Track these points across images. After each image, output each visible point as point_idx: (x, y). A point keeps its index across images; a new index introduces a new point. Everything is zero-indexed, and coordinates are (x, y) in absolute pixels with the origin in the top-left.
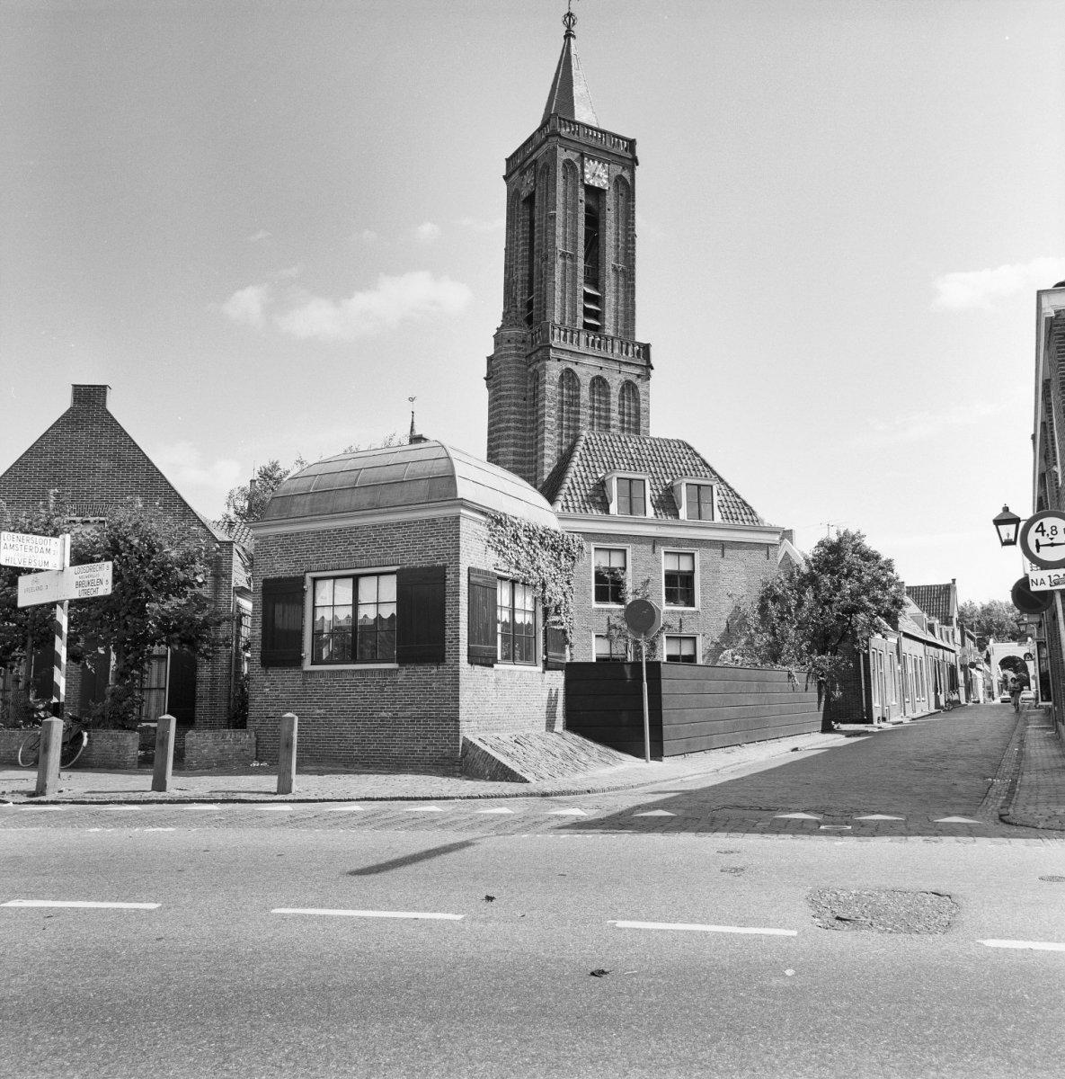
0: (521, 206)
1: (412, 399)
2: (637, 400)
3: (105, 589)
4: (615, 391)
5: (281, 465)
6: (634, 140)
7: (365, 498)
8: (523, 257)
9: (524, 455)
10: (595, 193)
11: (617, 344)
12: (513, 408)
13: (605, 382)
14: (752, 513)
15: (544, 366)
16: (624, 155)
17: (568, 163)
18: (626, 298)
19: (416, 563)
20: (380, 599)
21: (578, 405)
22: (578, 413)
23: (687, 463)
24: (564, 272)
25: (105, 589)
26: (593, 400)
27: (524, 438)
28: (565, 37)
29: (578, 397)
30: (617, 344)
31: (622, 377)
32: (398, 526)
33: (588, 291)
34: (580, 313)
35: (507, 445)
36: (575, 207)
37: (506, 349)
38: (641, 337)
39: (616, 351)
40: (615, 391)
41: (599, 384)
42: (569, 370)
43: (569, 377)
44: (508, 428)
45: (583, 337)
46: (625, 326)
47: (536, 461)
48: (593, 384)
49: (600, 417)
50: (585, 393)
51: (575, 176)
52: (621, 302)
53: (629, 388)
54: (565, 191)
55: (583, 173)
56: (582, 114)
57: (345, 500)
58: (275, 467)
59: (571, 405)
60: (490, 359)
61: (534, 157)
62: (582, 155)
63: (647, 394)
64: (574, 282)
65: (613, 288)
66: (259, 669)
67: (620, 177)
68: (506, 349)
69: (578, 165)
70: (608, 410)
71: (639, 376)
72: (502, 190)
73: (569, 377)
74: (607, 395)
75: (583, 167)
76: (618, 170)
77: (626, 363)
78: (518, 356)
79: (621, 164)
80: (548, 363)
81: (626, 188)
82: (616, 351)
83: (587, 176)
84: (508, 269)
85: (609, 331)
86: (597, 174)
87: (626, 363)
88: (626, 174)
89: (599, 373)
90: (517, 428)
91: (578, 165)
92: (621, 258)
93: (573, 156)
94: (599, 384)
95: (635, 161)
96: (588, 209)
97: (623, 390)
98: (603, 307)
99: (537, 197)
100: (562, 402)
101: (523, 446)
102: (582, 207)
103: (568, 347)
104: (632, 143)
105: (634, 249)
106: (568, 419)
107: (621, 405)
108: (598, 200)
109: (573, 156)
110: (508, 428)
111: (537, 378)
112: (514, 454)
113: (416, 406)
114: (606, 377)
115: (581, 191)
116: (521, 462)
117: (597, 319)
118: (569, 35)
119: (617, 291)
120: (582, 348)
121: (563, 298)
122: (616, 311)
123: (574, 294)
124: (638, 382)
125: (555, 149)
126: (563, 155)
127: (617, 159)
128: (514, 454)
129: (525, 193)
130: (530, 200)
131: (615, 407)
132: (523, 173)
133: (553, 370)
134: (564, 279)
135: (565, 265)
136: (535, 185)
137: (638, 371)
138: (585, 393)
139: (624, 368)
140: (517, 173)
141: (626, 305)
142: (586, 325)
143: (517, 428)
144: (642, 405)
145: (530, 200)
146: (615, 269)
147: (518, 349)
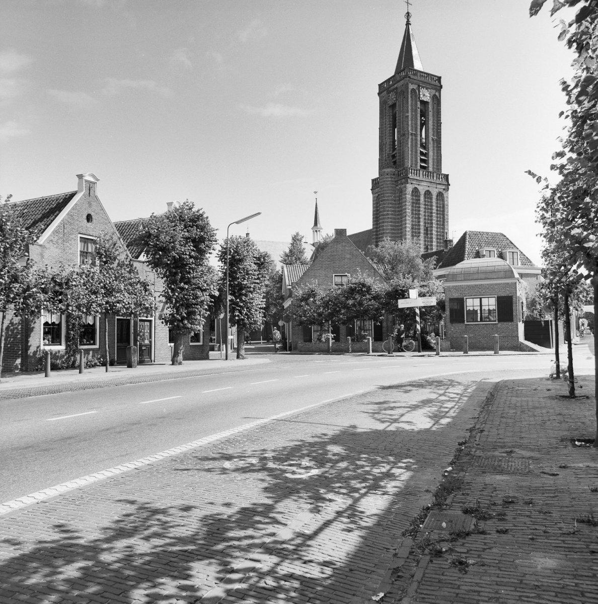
0: (387, 108)
1: (316, 192)
2: (443, 200)
3: (400, 301)
4: (434, 197)
5: (300, 234)
6: (440, 77)
7: (483, 276)
8: (389, 133)
9: (395, 226)
10: (424, 103)
11: (435, 175)
12: (390, 205)
13: (430, 193)
14: (531, 262)
15: (405, 187)
16: (435, 83)
17: (413, 89)
18: (437, 153)
19: (503, 295)
20: (490, 303)
21: (419, 204)
22: (420, 207)
23: (505, 243)
24: (412, 142)
25: (400, 301)
26: (425, 201)
27: (395, 219)
28: (406, 25)
29: (419, 200)
30: (435, 175)
31: (437, 190)
32: (496, 284)
33: (422, 150)
34: (419, 161)
35: (388, 222)
36: (416, 110)
37: (386, 178)
38: (444, 171)
39: (435, 178)
40: (434, 197)
41: (428, 194)
42: (416, 188)
43: (416, 191)
44: (388, 214)
45: (421, 172)
46: (437, 166)
47: (401, 229)
48: (425, 194)
49: (428, 209)
50: (422, 198)
51: (416, 96)
52: (435, 155)
53: (440, 196)
54: (412, 103)
55: (419, 94)
56: (418, 65)
57: (476, 277)
58: (298, 234)
59: (416, 204)
60: (375, 183)
61: (395, 86)
62: (419, 86)
63: (447, 197)
64: (416, 146)
65: (432, 148)
66: (449, 324)
67: (435, 95)
68: (386, 178)
69: (417, 91)
70: (432, 206)
71: (444, 189)
72: (377, 100)
73: (416, 191)
74: (431, 199)
75: (419, 91)
76: (433, 92)
77: (439, 184)
78: (391, 181)
79: (435, 89)
80: (407, 185)
81: (437, 100)
82: (435, 178)
83: (421, 96)
84: (381, 138)
85: (431, 169)
86: (426, 95)
87: (439, 184)
88: (437, 94)
89: (427, 189)
90: (392, 214)
91: (417, 91)
92: (435, 134)
93: (415, 87)
94: (428, 194)
95: (441, 87)
96: (421, 111)
97: (437, 196)
98: (428, 158)
99: (397, 105)
100: (413, 203)
101: (395, 222)
102: (419, 110)
103: (415, 178)
104: (440, 78)
105: (440, 129)
106: (416, 210)
107: (437, 203)
108: (425, 107)
109: (415, 87)
110: (388, 214)
111: (402, 192)
112: (391, 226)
113: (317, 196)
114: (431, 190)
115: (419, 103)
116: (394, 229)
117: (425, 163)
118: (408, 24)
119: (434, 150)
120: (421, 178)
121: (412, 154)
122: (433, 159)
123: (416, 152)
124: (444, 192)
125: (408, 84)
126: (411, 87)
127: (434, 87)
128: (391, 226)
129: (390, 103)
130: (393, 106)
131: (434, 204)
132: (389, 93)
133: (409, 188)
134: (412, 145)
135: (412, 139)
136: (397, 100)
137: (444, 187)
138: (422, 198)
139: (439, 186)
140: (385, 92)
141: (437, 156)
142: (421, 167)
143: (392, 214)
144: (446, 203)
145: (393, 106)
146: (433, 140)
147: (391, 178)
